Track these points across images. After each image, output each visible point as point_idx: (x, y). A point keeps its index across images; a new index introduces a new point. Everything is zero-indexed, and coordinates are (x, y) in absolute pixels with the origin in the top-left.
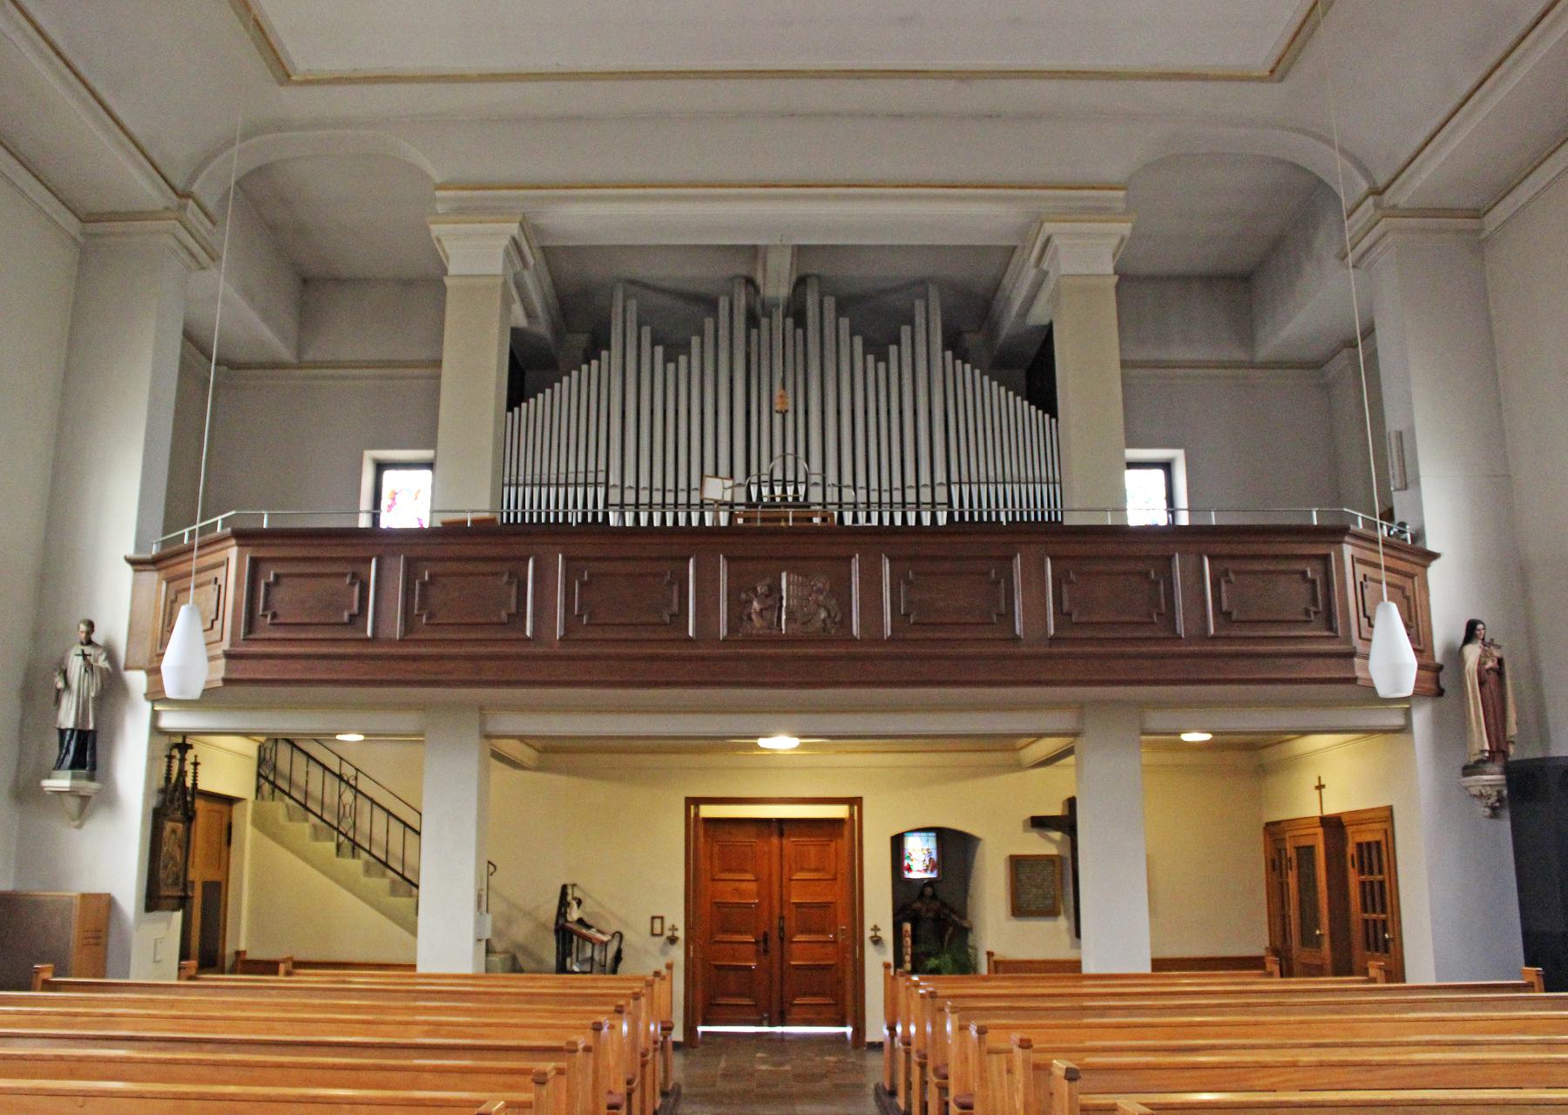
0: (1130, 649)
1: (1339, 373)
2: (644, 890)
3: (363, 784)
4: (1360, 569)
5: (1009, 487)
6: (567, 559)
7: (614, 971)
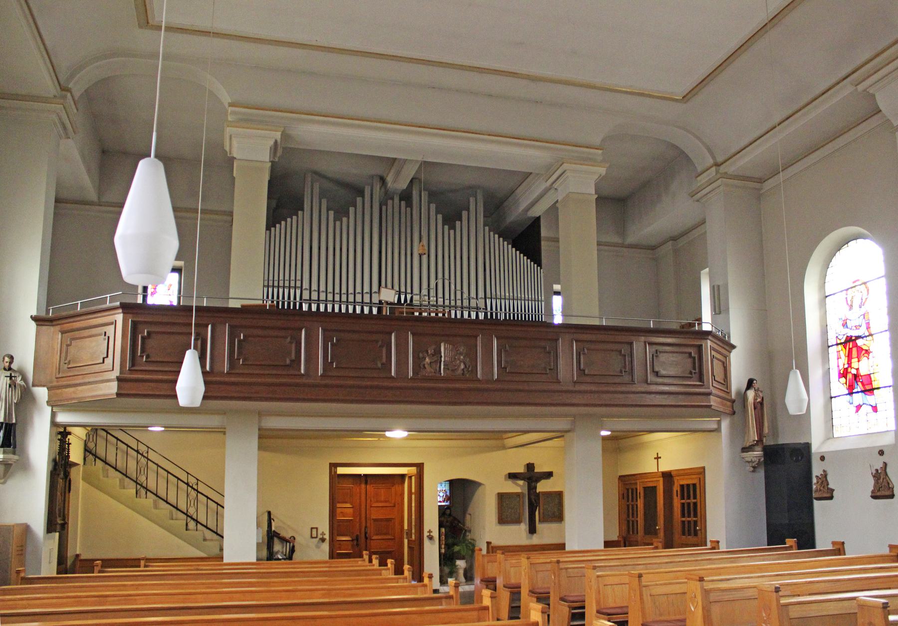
0: (611, 389)
1: (678, 256)
2: (310, 514)
3: (152, 455)
4: (713, 353)
5: (503, 302)
6: (324, 330)
7: (290, 558)
